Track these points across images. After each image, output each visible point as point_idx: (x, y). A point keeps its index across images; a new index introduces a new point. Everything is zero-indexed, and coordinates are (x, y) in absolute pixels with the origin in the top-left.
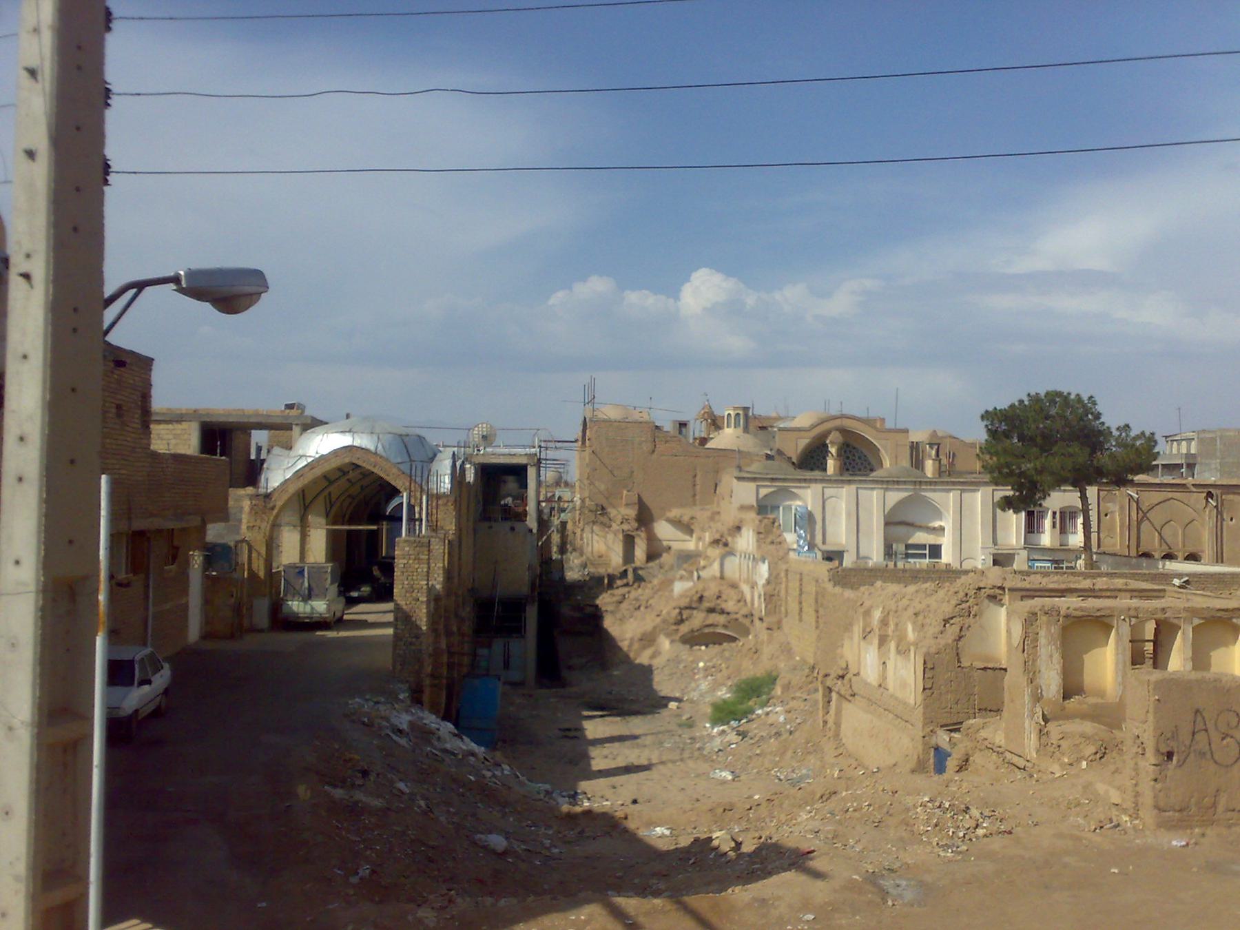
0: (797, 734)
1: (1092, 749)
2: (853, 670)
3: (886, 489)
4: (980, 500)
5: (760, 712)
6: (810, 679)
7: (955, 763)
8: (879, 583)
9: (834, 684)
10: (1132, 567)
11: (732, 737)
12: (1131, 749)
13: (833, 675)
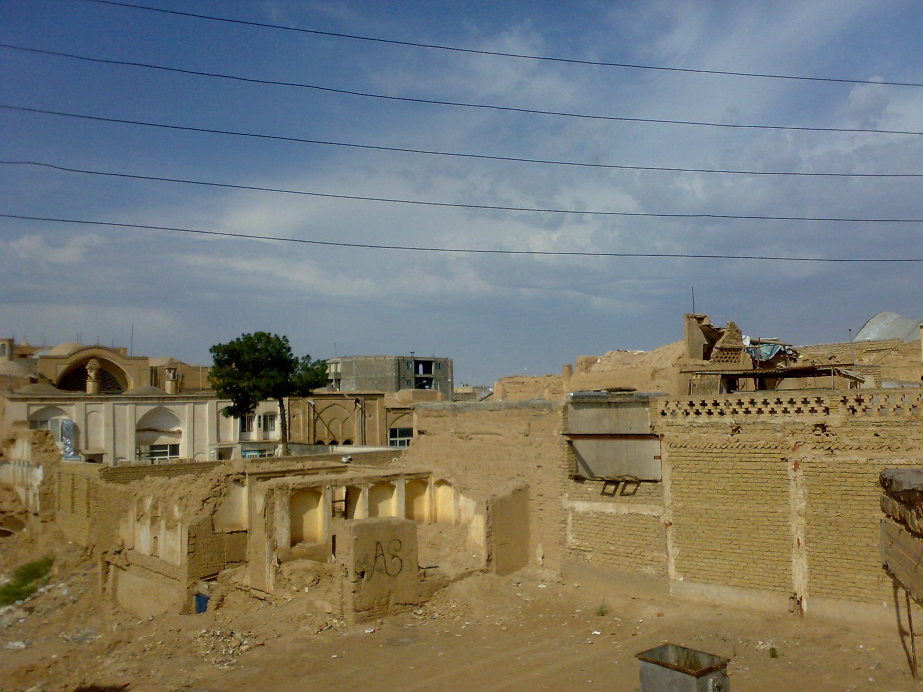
0: (80, 602)
1: (311, 578)
2: (128, 546)
3: (137, 404)
4: (208, 409)
5: (42, 590)
6: (83, 558)
7: (215, 603)
8: (148, 478)
9: (113, 559)
10: (311, 452)
11: (21, 613)
12: (339, 573)
13: (111, 551)
